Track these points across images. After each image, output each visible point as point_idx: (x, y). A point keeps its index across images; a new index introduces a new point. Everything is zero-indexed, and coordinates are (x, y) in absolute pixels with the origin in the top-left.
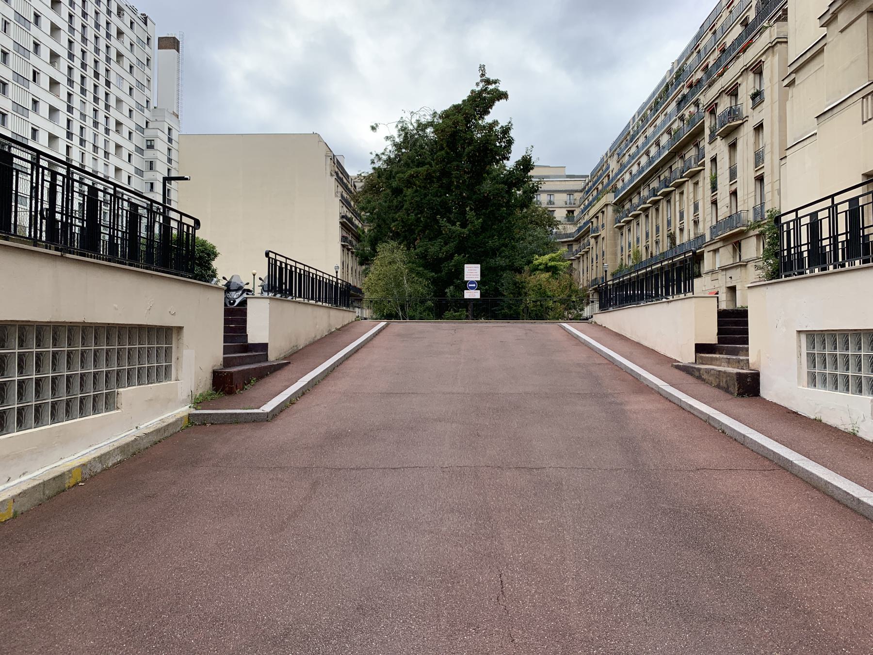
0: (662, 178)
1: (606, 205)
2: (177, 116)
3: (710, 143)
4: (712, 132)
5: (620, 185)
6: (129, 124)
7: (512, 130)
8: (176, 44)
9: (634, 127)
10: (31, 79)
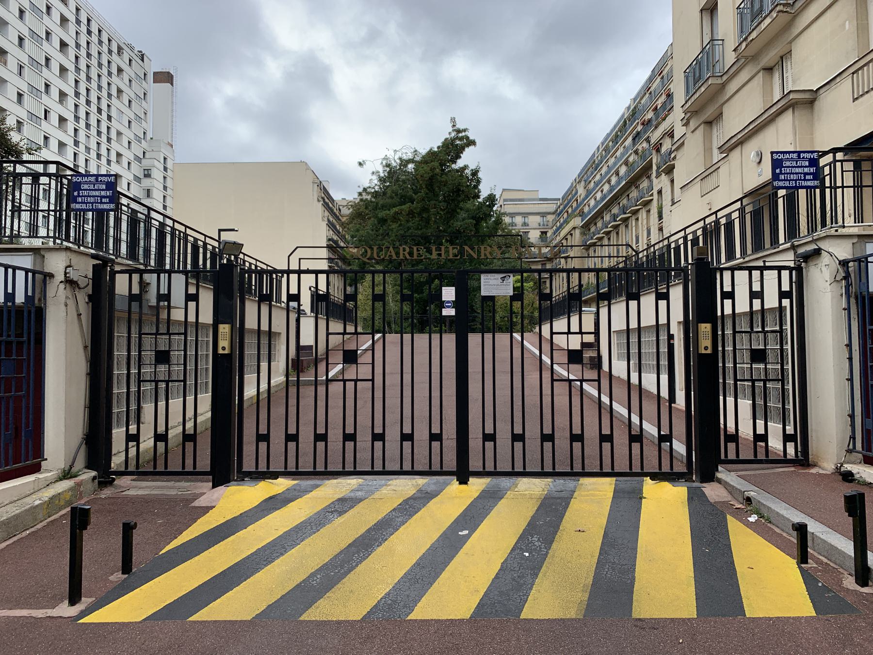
0: (621, 205)
1: (574, 228)
2: (172, 146)
3: (657, 177)
4: (658, 168)
5: (586, 209)
6: (128, 155)
7: (480, 172)
8: (170, 78)
9: (598, 157)
10: (43, 117)
